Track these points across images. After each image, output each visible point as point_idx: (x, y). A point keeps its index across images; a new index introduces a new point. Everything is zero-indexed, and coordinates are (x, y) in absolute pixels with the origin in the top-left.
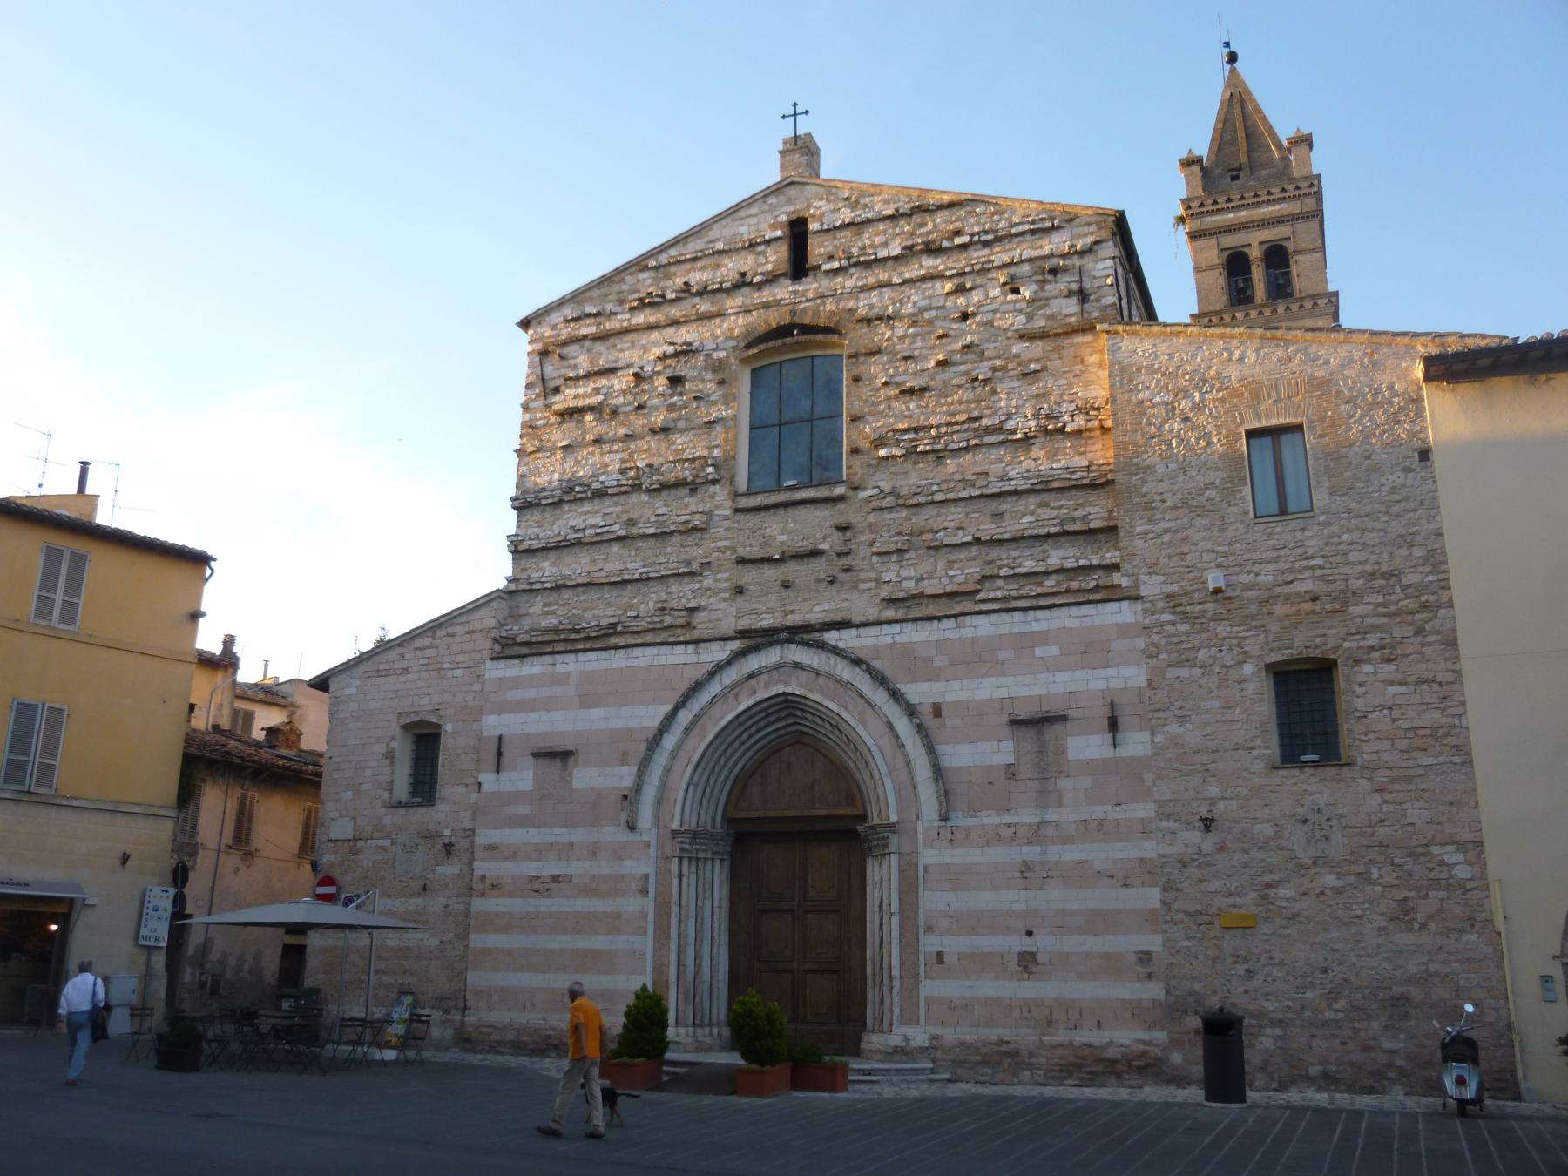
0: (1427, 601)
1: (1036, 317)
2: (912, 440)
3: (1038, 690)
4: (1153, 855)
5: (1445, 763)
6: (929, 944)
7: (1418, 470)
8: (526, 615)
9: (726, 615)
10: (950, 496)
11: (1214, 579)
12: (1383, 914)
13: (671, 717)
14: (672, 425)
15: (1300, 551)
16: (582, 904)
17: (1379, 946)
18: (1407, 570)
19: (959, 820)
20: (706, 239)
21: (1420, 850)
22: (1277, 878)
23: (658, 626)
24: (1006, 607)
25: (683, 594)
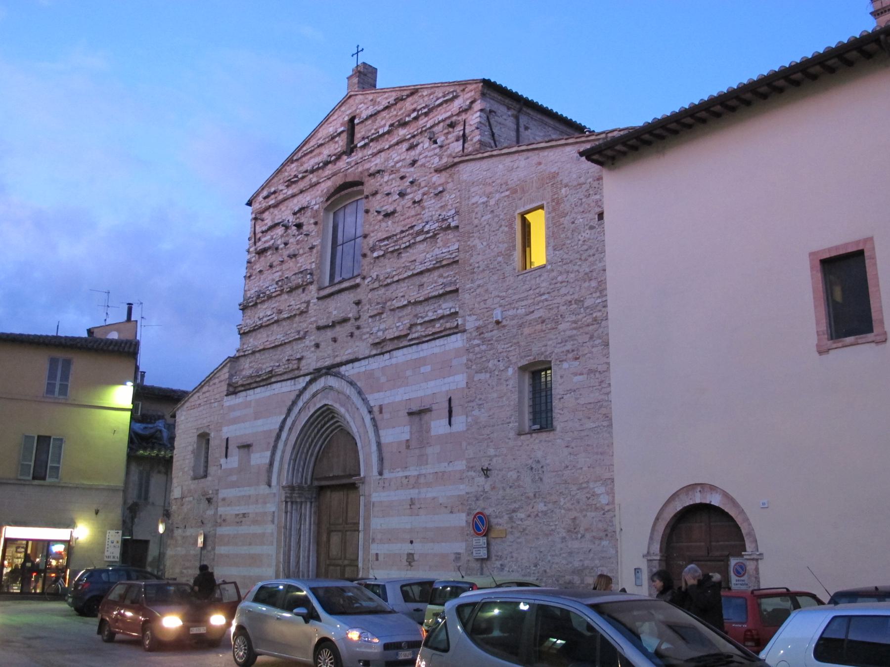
0: (596, 316)
1: (443, 157)
2: (386, 245)
3: (420, 394)
4: (463, 493)
5: (599, 426)
7: (597, 227)
8: (243, 369)
9: (312, 362)
10: (401, 277)
11: (498, 315)
12: (564, 528)
13: (284, 421)
14: (297, 253)
15: (537, 291)
17: (561, 549)
18: (588, 297)
19: (387, 475)
20: (317, 138)
21: (584, 485)
22: (517, 506)
23: (287, 370)
25: (297, 350)
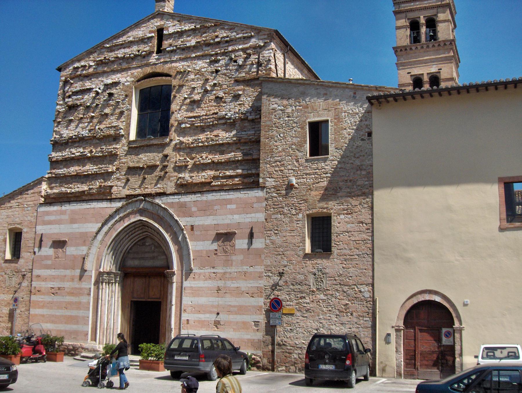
6: (185, 317)
16: (68, 299)
24: (221, 189)
